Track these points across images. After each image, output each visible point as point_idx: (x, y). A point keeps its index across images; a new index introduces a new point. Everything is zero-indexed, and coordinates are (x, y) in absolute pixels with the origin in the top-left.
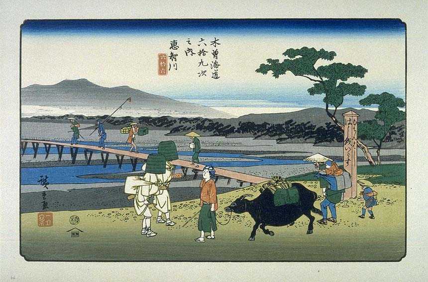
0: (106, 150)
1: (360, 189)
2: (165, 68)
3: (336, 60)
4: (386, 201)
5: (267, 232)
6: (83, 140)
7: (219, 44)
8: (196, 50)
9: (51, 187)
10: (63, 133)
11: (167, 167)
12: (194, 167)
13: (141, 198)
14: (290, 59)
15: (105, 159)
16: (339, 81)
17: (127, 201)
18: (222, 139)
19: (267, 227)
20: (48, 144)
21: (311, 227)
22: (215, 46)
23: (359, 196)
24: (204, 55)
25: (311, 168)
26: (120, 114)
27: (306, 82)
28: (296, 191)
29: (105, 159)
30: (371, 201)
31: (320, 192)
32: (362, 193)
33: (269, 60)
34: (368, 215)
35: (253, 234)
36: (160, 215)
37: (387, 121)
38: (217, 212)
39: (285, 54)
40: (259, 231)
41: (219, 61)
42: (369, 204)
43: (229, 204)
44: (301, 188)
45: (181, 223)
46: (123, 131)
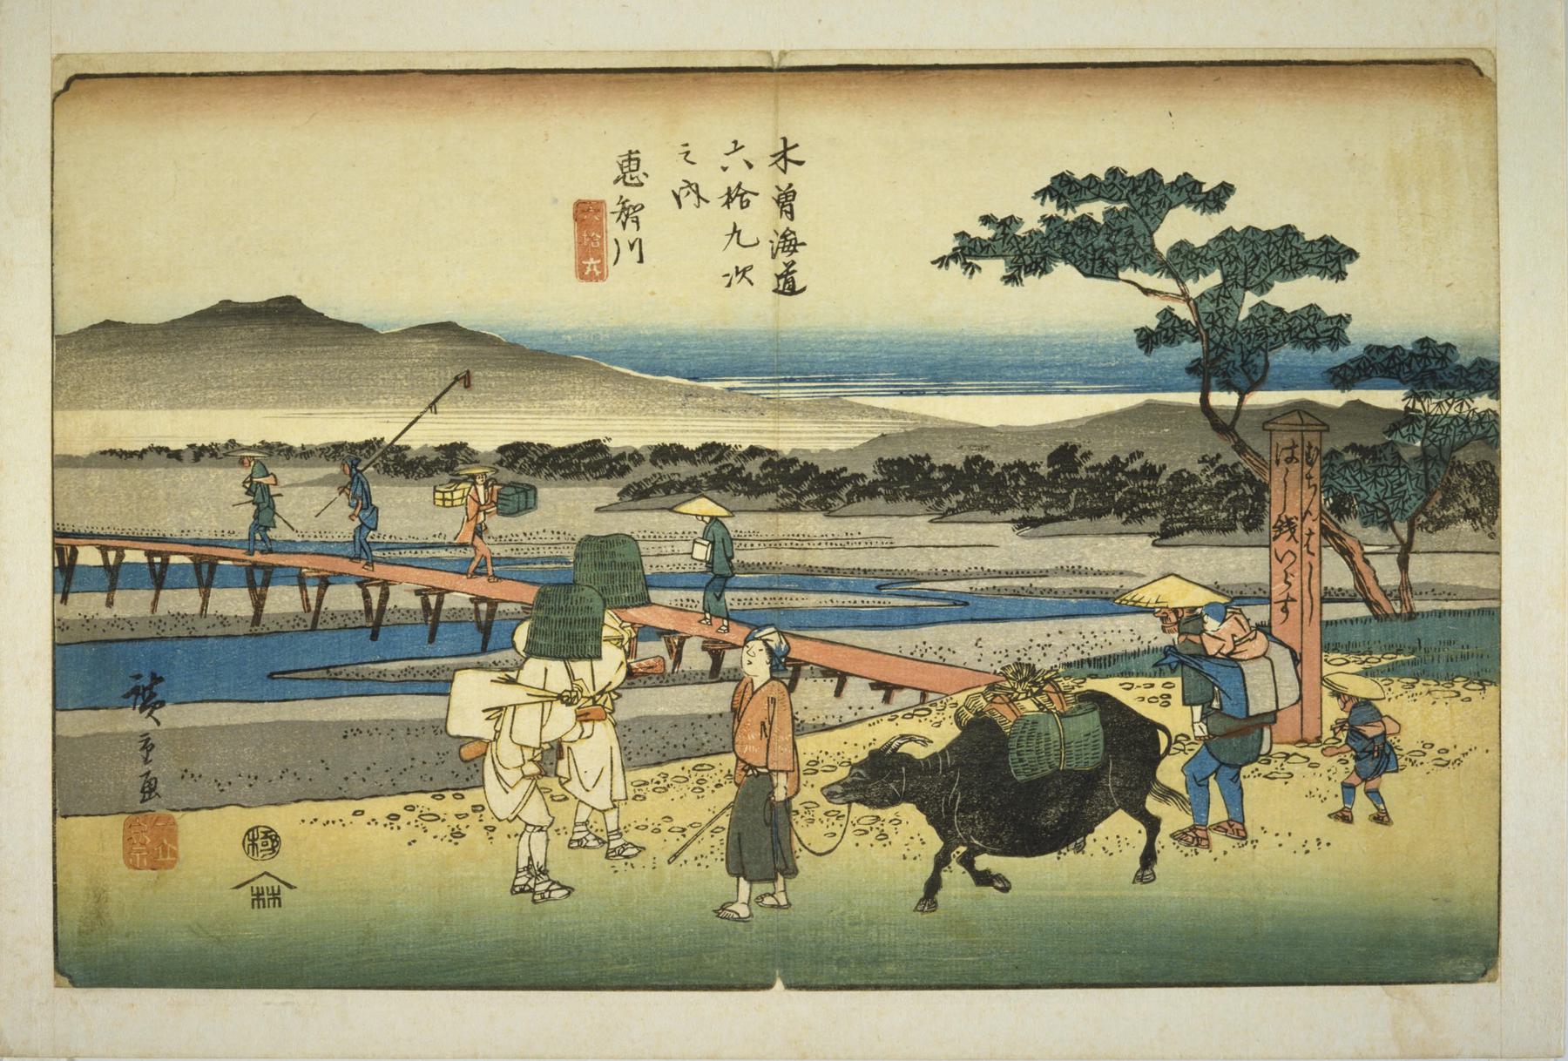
0: (381, 572)
1: (1333, 711)
2: (599, 254)
3: (1236, 215)
4: (1433, 753)
5: (984, 879)
6: (289, 535)
7: (800, 163)
8: (714, 188)
9: (171, 716)
10: (212, 508)
11: (606, 632)
12: (709, 632)
13: (508, 753)
14: (1061, 213)
15: (375, 606)
16: (1251, 299)
17: (461, 766)
18: (812, 523)
19: (983, 862)
20: (158, 553)
21: (1149, 857)
22: (784, 171)
23: (1327, 734)
24: (745, 205)
25: (1151, 633)
26: (427, 436)
27: (1113, 307)
28: (1090, 722)
29: (375, 606)
30: (1373, 752)
31: (1178, 718)
32: (1340, 725)
33: (986, 220)
34: (1362, 806)
35: (933, 885)
36: (582, 817)
37: (1421, 440)
38: (796, 804)
39: (1043, 193)
40: (955, 876)
41: (801, 227)
42: (1370, 765)
43: (843, 773)
44: (1101, 701)
45: (659, 846)
46: (444, 500)
